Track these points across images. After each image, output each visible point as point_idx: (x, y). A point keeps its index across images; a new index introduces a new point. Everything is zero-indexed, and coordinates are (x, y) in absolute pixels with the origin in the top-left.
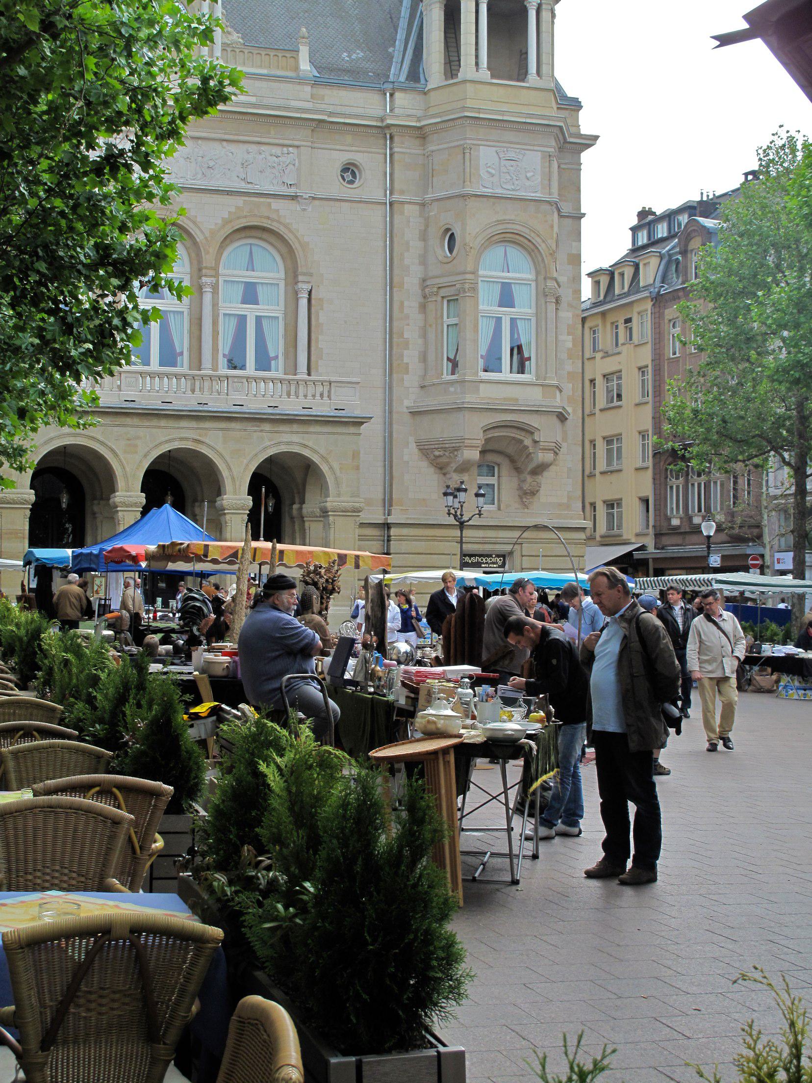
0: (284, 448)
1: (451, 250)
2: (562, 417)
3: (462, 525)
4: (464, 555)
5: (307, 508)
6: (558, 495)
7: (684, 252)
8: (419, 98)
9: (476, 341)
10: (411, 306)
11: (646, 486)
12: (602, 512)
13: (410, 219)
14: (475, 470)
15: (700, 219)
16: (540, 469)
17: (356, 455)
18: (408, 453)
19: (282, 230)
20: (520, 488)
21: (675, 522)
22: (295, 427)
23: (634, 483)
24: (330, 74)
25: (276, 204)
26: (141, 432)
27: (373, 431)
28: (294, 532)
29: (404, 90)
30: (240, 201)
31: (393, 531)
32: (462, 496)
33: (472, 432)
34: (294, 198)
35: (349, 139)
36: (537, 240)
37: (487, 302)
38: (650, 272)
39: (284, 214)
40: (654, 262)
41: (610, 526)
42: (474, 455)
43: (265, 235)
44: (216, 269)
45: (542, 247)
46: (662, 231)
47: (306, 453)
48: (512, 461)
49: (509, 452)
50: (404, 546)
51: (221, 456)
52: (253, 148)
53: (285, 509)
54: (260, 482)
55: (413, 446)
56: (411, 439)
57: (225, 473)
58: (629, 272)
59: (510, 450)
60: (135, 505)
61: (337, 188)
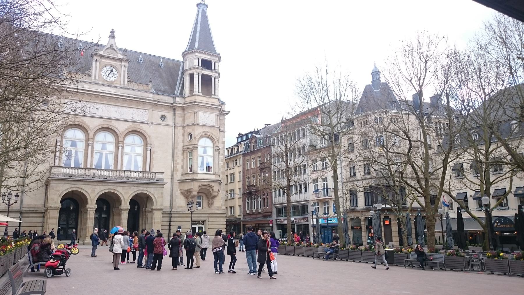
0: (140, 192)
1: (191, 139)
2: (220, 183)
3: (192, 213)
4: (192, 221)
5: (147, 209)
6: (219, 203)
7: (250, 143)
8: (183, 99)
9: (197, 163)
10: (180, 153)
11: (240, 202)
12: (229, 209)
13: (179, 131)
14: (196, 198)
15: (255, 135)
16: (215, 197)
17: (162, 193)
18: (177, 193)
19: (143, 132)
20: (208, 203)
21: (248, 212)
22: (144, 186)
23: (237, 202)
24: (159, 92)
25: (142, 125)
26: (97, 187)
27: (167, 187)
28: (143, 216)
29: (178, 96)
30: (131, 124)
31: (172, 215)
32: (193, 205)
33: (195, 186)
34: (147, 124)
35: (163, 108)
36: (214, 137)
37: (200, 151)
38: (242, 148)
39: (144, 128)
40: (243, 145)
41: (231, 213)
42: (195, 193)
43: (138, 133)
44: (123, 142)
45: (215, 139)
46: (244, 138)
47: (147, 193)
48: (206, 195)
49: (207, 193)
50: (175, 219)
51: (121, 193)
52: (135, 110)
53: (141, 209)
54: (133, 202)
55: (179, 191)
56: (179, 190)
57: (122, 199)
58: (236, 148)
59: (206, 192)
60: (94, 208)
61: (160, 121)
